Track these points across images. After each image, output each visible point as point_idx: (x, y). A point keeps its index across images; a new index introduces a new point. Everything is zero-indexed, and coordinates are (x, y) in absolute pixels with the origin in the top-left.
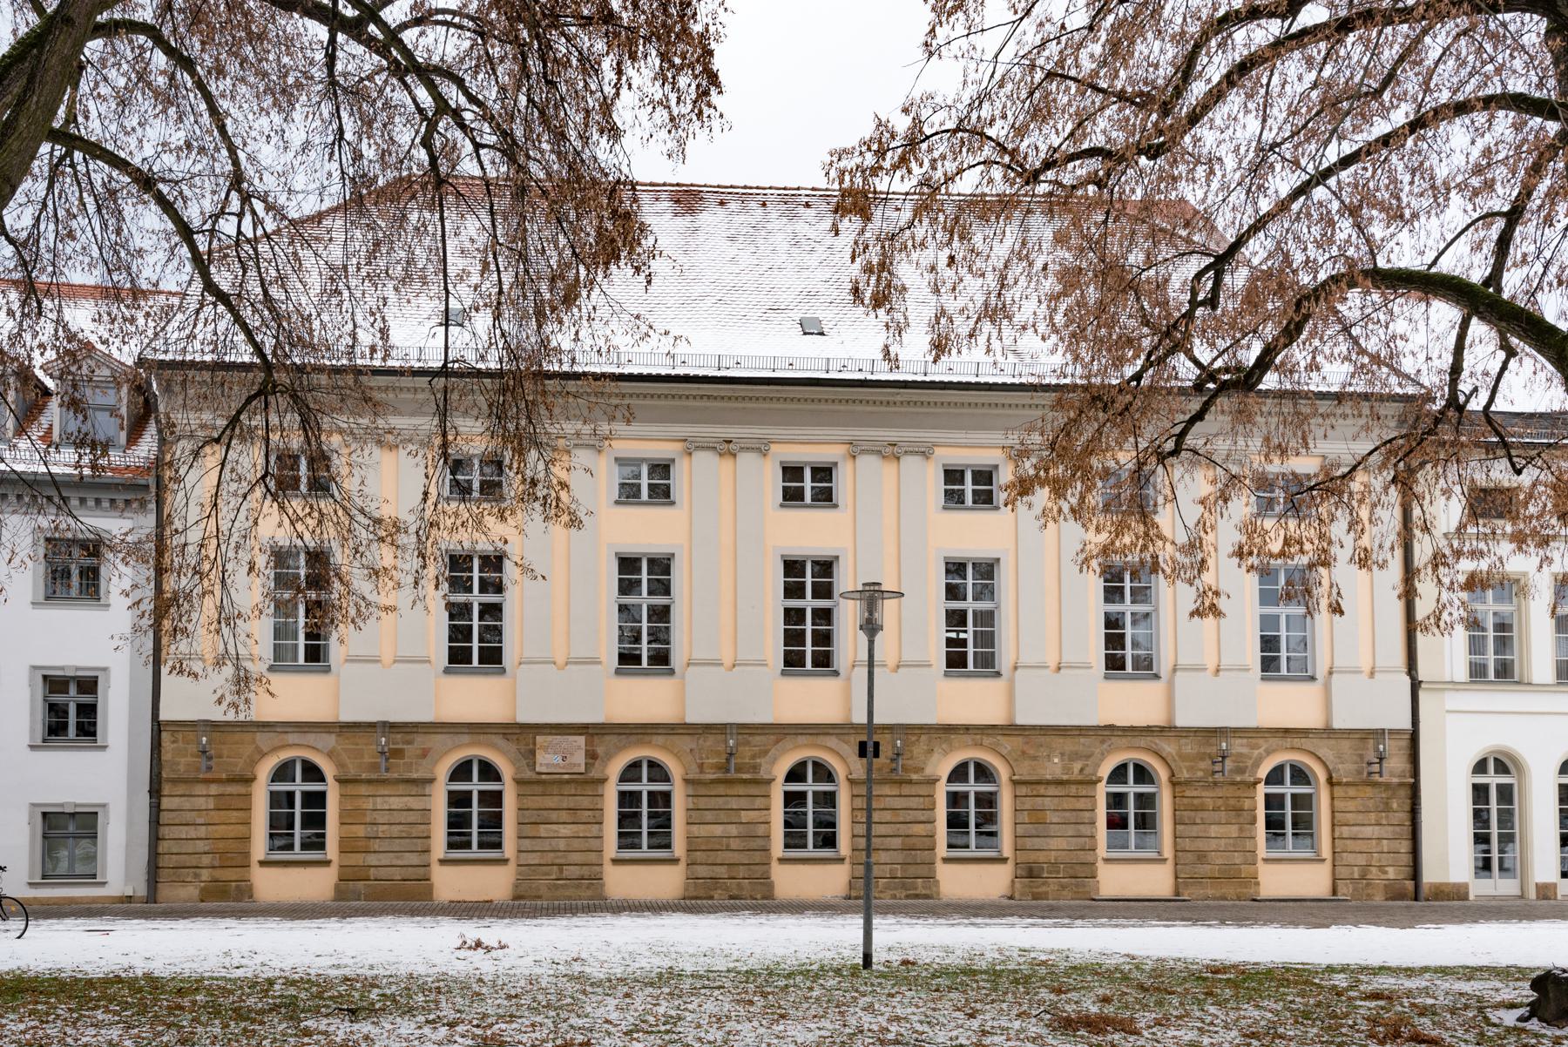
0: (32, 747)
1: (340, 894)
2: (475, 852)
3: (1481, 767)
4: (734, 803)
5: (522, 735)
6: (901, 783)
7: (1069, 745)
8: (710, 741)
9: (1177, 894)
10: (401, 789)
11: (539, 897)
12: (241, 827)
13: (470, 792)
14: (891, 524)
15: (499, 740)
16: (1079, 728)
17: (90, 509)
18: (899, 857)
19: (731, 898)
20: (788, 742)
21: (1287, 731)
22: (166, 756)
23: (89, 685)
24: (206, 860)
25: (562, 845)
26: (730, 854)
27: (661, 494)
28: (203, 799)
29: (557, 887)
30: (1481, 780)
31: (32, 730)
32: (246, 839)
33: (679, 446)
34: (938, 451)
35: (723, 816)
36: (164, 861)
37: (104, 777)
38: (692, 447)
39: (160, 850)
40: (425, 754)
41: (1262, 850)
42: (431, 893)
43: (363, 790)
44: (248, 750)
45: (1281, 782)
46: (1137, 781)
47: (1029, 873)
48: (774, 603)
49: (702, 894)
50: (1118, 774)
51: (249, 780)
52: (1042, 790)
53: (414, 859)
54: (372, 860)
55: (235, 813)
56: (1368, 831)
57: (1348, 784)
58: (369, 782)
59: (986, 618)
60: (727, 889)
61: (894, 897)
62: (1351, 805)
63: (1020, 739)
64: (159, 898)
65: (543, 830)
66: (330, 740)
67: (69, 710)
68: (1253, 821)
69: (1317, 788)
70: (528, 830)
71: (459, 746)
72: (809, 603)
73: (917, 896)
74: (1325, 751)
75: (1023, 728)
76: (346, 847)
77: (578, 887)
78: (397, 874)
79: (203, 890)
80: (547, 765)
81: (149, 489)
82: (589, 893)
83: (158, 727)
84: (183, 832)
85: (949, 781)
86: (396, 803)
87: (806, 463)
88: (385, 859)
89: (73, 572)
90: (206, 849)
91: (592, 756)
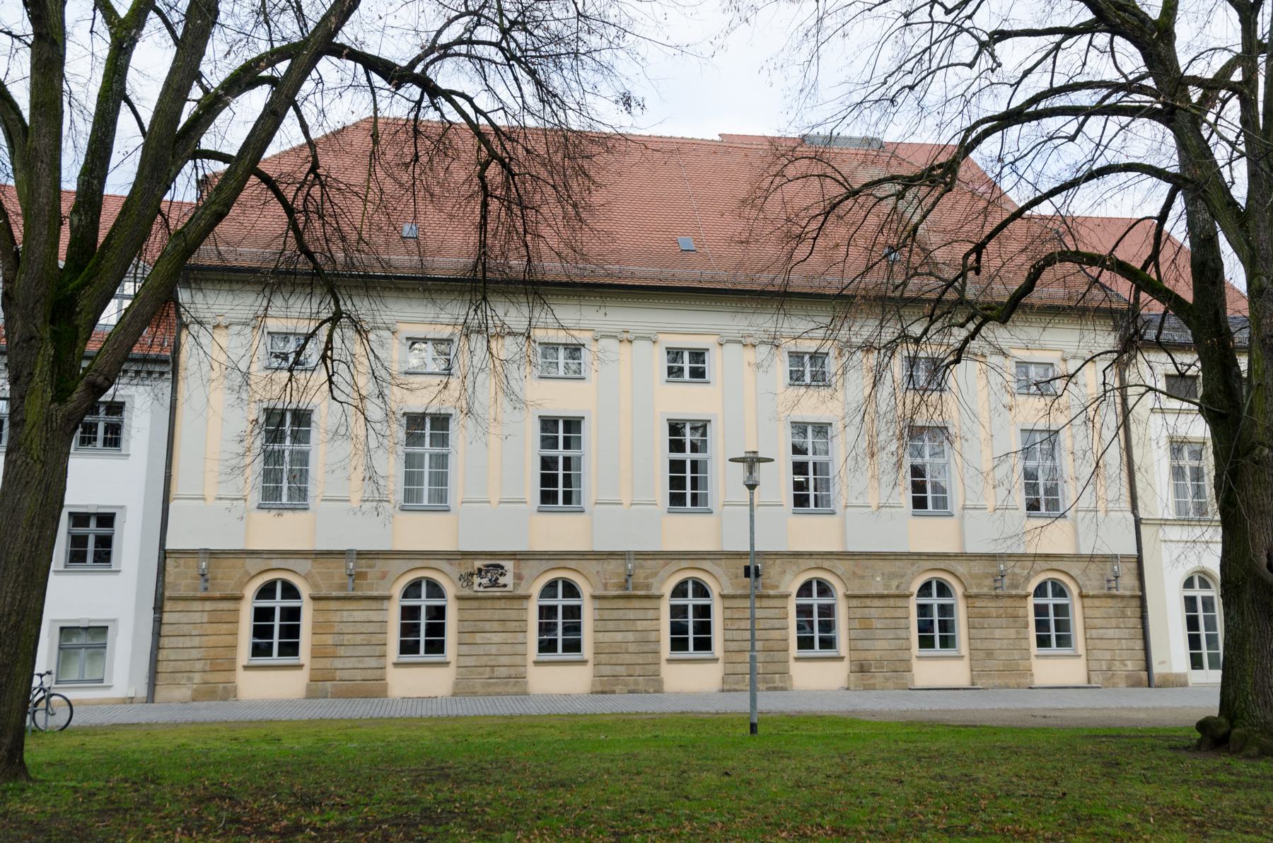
3: (1189, 583)
4: (631, 615)
7: (888, 566)
21: (1047, 556)
22: (169, 579)
23: (107, 520)
24: (199, 665)
25: (493, 649)
28: (198, 613)
29: (489, 685)
30: (1190, 593)
32: (234, 647)
40: (383, 576)
43: (333, 605)
45: (1045, 595)
52: (868, 602)
53: (372, 663)
55: (225, 626)
56: (1111, 633)
57: (1094, 597)
60: (626, 685)
62: (1097, 613)
63: (851, 562)
65: (479, 638)
66: (305, 565)
68: (1026, 626)
69: (1072, 600)
72: (560, 452)
77: (506, 684)
78: (358, 675)
83: (164, 554)
84: (180, 642)
86: (359, 616)
88: (349, 663)
90: (199, 656)
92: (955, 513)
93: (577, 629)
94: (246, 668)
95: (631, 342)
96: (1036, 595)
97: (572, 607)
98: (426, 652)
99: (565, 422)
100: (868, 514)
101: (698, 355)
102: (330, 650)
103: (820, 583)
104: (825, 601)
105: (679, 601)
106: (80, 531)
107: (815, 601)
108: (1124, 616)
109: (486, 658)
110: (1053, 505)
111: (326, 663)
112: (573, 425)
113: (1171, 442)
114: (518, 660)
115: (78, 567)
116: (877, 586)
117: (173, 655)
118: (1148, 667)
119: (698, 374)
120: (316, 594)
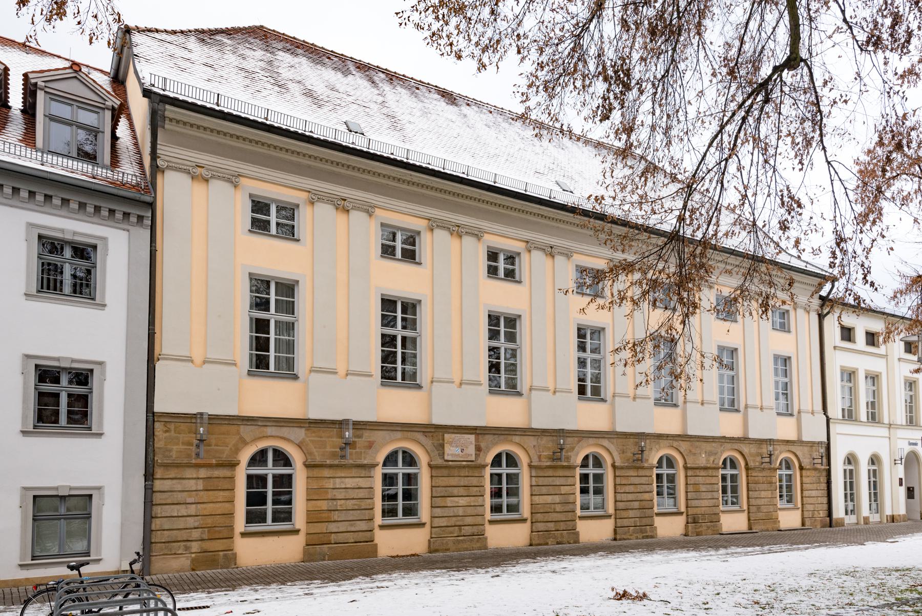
0: (24, 433)
1: (308, 556)
2: (270, 525)
4: (558, 481)
5: (435, 432)
6: (638, 468)
7: (708, 447)
8: (545, 441)
9: (750, 528)
10: (354, 472)
11: (447, 550)
12: (227, 505)
13: (396, 474)
14: (548, 298)
15: (420, 436)
16: (713, 438)
17: (73, 211)
18: (637, 513)
19: (558, 543)
20: (584, 442)
22: (158, 444)
23: (82, 377)
24: (196, 534)
25: (461, 511)
26: (555, 515)
27: (410, 256)
28: (193, 481)
29: (459, 541)
31: (24, 418)
32: (231, 515)
33: (304, 195)
34: (575, 256)
35: (552, 490)
36: (157, 537)
37: (100, 462)
38: (530, 246)
39: (153, 527)
40: (370, 445)
41: (379, 519)
42: (376, 551)
43: (326, 473)
44: (232, 440)
46: (275, 464)
47: (693, 520)
48: (375, 330)
49: (542, 542)
50: (391, 460)
51: (233, 465)
52: (698, 472)
53: (362, 526)
54: (333, 527)
55: (221, 493)
57: (809, 469)
58: (331, 466)
59: (289, 328)
60: (555, 537)
61: (637, 538)
63: (688, 443)
64: (153, 570)
65: (449, 501)
66: (299, 434)
67: (61, 398)
69: (740, 471)
70: (439, 502)
71: (392, 441)
73: (647, 537)
74: (746, 449)
75: (691, 437)
76: (313, 518)
77: (472, 540)
78: (351, 537)
79: (193, 560)
80: (452, 455)
81: (137, 205)
82: (478, 545)
83: (152, 416)
84: (175, 511)
85: (384, 465)
86: (350, 483)
87: (502, 250)
88: (342, 527)
89: (64, 271)
90: (196, 524)
91: (478, 449)
92: (524, 392)
93: (513, 492)
94: (244, 535)
95: (207, 181)
96: (493, 465)
97: (282, 476)
98: (273, 521)
99: (277, 283)
100: (631, 405)
101: (511, 258)
102: (325, 515)
103: (509, 456)
104: (598, 471)
105: (257, 471)
106: (48, 387)
107: (504, 470)
108: (820, 483)
109: (454, 519)
110: (596, 391)
111: (321, 528)
112: (410, 307)
113: (251, 279)
114: (478, 520)
115: (48, 428)
116: (702, 460)
117: (167, 525)
118: (830, 514)
119: (510, 275)
120: (309, 461)
